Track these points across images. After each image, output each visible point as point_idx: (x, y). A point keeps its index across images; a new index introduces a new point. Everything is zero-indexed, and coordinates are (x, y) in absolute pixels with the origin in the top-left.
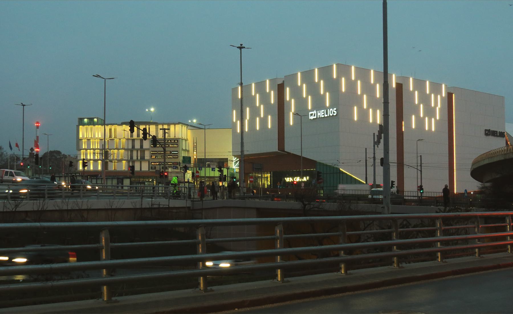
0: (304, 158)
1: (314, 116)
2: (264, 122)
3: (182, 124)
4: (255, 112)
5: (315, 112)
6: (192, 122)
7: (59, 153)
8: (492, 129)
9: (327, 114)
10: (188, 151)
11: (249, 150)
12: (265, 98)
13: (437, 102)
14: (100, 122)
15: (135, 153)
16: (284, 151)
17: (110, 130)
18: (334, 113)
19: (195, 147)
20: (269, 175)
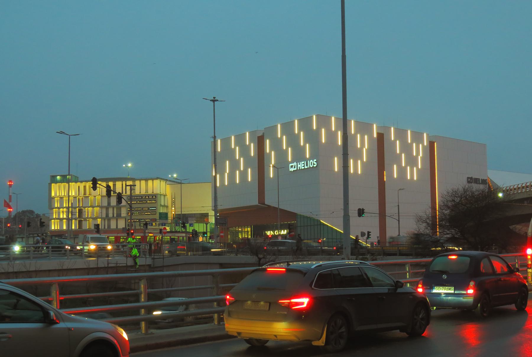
0: (282, 210)
1: (295, 167)
2: (243, 175)
3: (161, 179)
4: (235, 165)
5: (295, 164)
6: (172, 176)
7: (32, 212)
8: (474, 177)
9: (307, 165)
10: (167, 207)
11: (223, 205)
12: (245, 151)
13: (419, 151)
14: (73, 179)
15: (110, 210)
16: (264, 204)
17: (85, 187)
18: (314, 164)
19: (173, 203)
20: (249, 229)
